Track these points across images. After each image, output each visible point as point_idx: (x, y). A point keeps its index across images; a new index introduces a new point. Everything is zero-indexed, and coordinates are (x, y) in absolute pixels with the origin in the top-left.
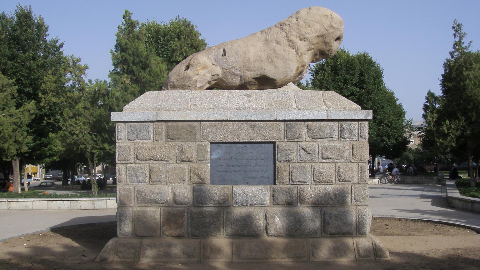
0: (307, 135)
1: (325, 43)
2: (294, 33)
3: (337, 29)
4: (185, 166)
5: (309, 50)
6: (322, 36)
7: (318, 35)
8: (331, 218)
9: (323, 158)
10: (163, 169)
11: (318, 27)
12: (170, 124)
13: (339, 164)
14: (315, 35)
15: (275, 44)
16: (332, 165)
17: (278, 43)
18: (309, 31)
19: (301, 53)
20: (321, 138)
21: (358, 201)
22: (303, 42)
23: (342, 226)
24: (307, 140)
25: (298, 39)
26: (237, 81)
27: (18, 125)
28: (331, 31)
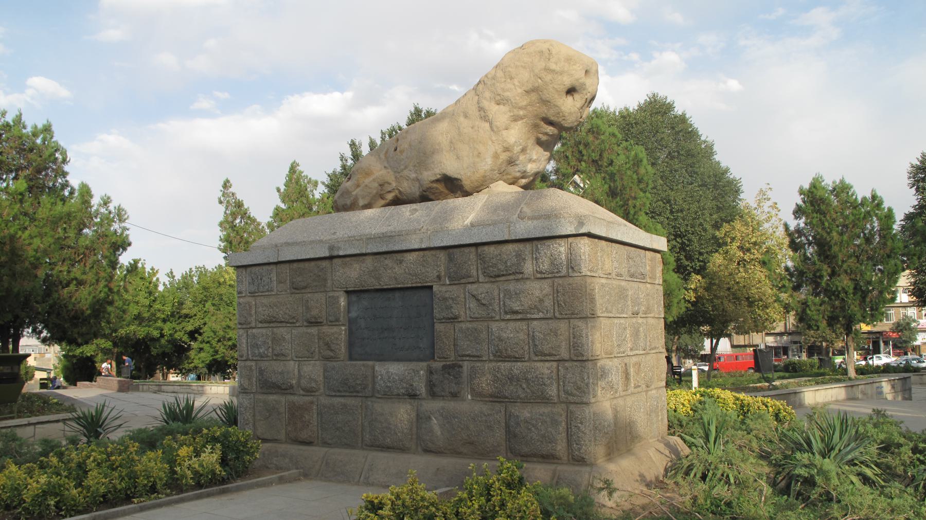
0: (480, 272)
1: (545, 102)
2: (487, 94)
3: (561, 73)
4: (314, 330)
5: (516, 119)
6: (535, 90)
7: (526, 89)
8: (518, 424)
9: (506, 313)
10: (288, 337)
11: (525, 75)
12: (295, 265)
13: (535, 322)
14: (519, 91)
15: (462, 119)
16: (523, 325)
17: (466, 116)
18: (510, 86)
19: (498, 128)
20: (503, 275)
21: (569, 395)
22: (502, 107)
23: (538, 440)
24: (480, 280)
25: (493, 103)
26: (416, 191)
27: (760, 476)
28: (548, 78)
